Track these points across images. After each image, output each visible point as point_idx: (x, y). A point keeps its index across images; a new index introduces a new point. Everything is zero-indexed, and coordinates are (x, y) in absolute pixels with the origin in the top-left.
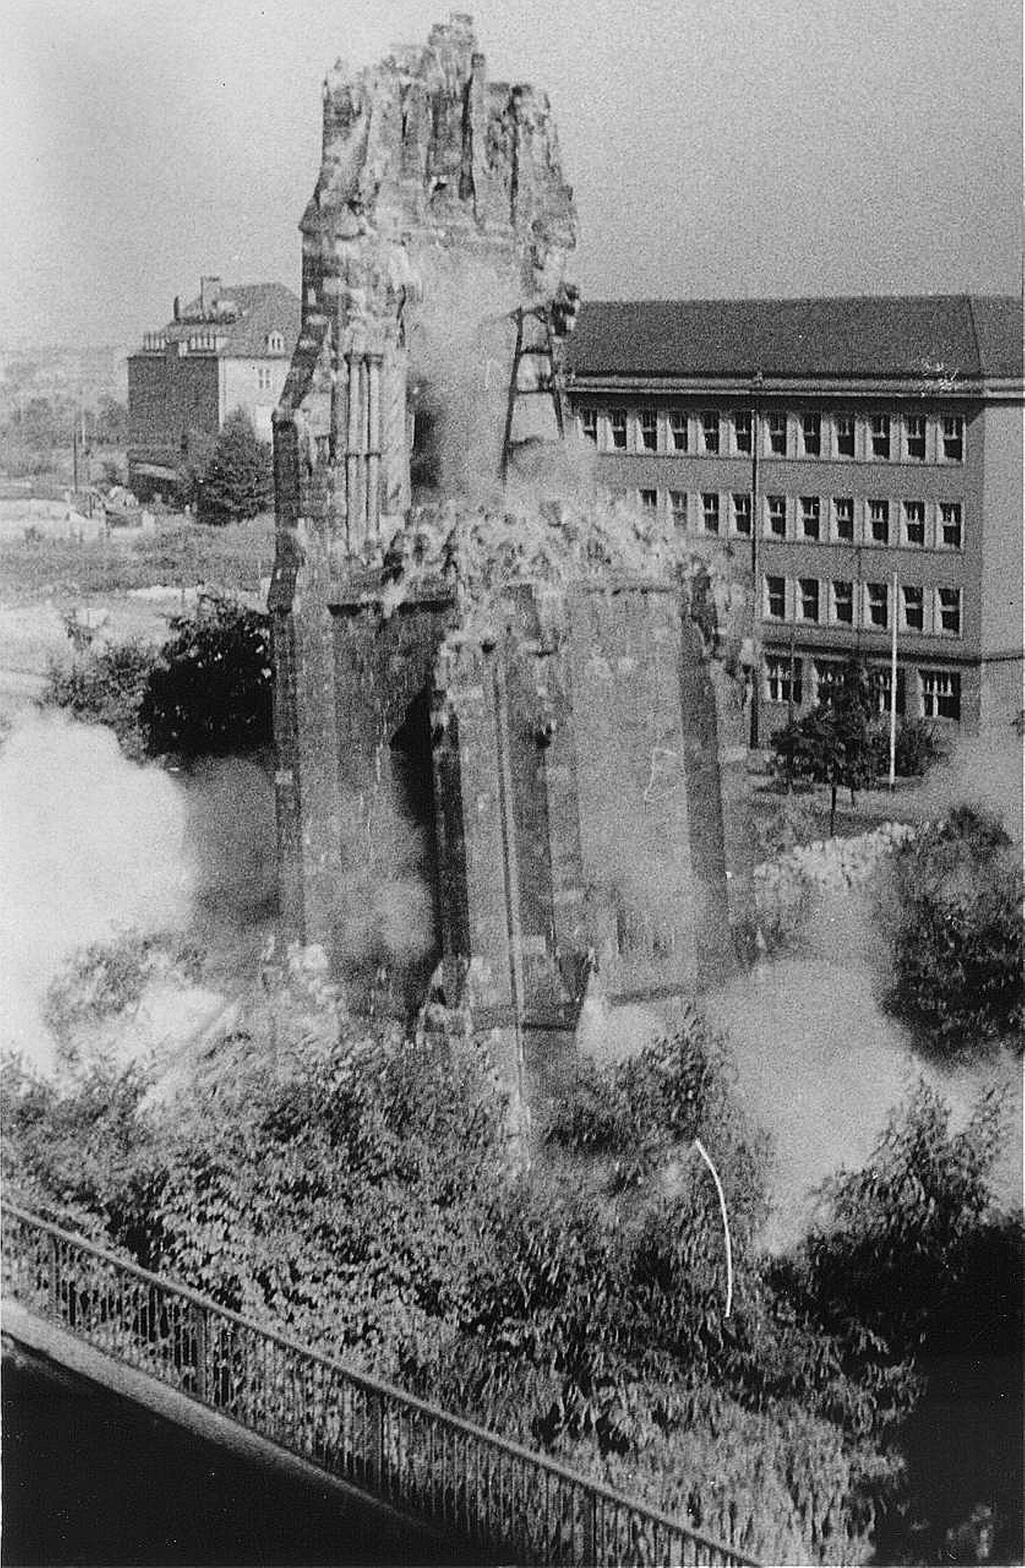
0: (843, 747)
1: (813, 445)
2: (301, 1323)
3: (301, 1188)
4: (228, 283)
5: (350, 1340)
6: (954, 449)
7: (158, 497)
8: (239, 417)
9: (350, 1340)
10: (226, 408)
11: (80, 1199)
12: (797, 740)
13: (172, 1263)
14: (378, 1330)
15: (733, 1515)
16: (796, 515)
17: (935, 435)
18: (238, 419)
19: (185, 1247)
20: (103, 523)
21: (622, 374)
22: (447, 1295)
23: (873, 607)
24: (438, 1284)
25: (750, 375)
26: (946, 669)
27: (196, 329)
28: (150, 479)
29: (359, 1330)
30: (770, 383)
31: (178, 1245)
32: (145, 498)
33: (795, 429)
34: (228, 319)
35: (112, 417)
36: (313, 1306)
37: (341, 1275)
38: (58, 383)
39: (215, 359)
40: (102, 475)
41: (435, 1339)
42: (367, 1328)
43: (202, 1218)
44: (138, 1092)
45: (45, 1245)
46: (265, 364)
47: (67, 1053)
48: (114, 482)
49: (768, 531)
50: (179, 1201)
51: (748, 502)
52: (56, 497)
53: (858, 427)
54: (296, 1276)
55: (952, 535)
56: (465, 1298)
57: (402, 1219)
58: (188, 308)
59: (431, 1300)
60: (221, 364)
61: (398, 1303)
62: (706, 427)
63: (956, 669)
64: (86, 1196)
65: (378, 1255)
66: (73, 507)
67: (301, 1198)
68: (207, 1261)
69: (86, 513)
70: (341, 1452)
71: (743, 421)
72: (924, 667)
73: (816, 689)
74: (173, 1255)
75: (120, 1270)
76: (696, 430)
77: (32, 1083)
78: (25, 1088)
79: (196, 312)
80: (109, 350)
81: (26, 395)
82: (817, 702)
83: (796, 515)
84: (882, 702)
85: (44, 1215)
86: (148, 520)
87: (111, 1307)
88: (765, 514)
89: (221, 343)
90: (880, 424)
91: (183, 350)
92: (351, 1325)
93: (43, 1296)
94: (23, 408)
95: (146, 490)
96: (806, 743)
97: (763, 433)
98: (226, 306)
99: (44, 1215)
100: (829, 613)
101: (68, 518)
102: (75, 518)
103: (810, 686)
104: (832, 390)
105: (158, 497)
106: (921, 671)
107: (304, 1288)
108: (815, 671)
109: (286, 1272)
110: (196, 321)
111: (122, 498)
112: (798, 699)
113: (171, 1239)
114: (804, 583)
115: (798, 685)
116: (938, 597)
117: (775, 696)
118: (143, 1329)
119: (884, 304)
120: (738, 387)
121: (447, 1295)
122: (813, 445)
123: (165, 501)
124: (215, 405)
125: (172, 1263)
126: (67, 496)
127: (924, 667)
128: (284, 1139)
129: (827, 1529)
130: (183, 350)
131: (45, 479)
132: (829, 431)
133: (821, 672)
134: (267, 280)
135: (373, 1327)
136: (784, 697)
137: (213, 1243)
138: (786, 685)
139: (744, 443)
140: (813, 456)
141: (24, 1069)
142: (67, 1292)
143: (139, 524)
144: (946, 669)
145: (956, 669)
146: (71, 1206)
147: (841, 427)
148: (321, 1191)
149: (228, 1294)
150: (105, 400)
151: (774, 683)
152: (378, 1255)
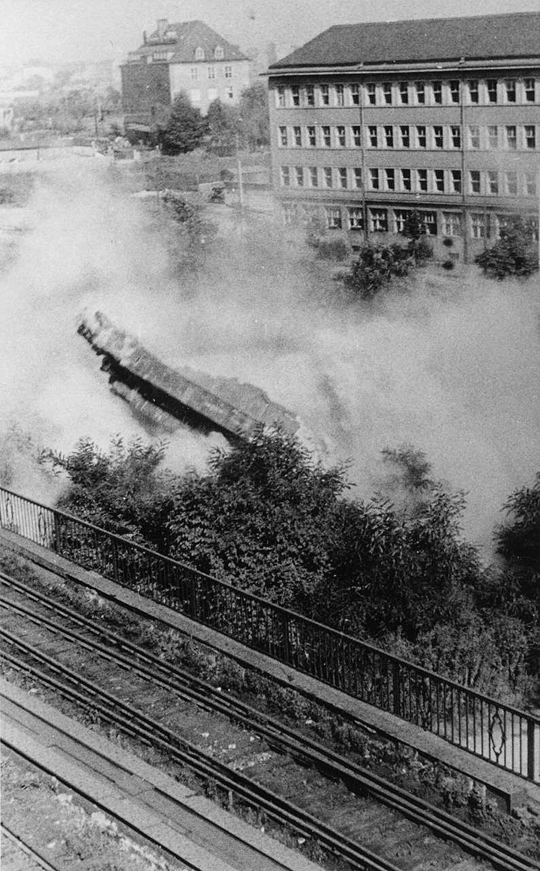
0: (514, 262)
1: (493, 97)
2: (242, 577)
3: (240, 508)
4: (171, 22)
5: (269, 584)
6: (531, 96)
7: (141, 141)
8: (181, 96)
9: (269, 584)
10: (174, 91)
11: (126, 518)
12: (488, 259)
13: (176, 548)
14: (283, 579)
15: (471, 669)
16: (431, 136)
17: (521, 89)
18: (182, 97)
19: (181, 541)
20: (113, 157)
21: (389, 63)
22: (318, 560)
23: (473, 183)
24: (313, 555)
25: (458, 59)
26: (429, 209)
27: (157, 48)
28: (137, 132)
29: (273, 580)
30: (469, 63)
31: (178, 539)
32: (134, 142)
33: (483, 89)
34: (173, 42)
35: (114, 97)
36: (249, 568)
37: (262, 552)
38: (84, 82)
39: (167, 65)
40: (112, 131)
41: (312, 582)
42: (277, 578)
43: (191, 526)
44: (155, 462)
45: (109, 542)
46: (194, 66)
47: (117, 443)
48: (118, 134)
49: (369, 144)
50: (179, 518)
51: (459, 130)
52: (87, 144)
53: (518, 85)
54: (240, 553)
55: (531, 142)
56: (327, 562)
57: (292, 523)
58: (152, 36)
59: (310, 563)
60: (171, 67)
61: (292, 566)
62: (453, 89)
63: (434, 210)
64: (129, 515)
65: (281, 542)
66: (96, 149)
67: (240, 514)
68: (193, 548)
69: (104, 152)
70: (267, 643)
71: (454, 86)
72: (396, 208)
73: (498, 231)
74: (176, 544)
75: (148, 554)
76: (380, 92)
77: (99, 458)
78: (95, 461)
79: (156, 39)
80: (109, 62)
81: (67, 89)
82: (499, 238)
83: (431, 136)
84: (534, 236)
85: (108, 527)
86: (137, 155)
87: (145, 572)
88: (367, 134)
89: (169, 56)
90: (371, 87)
91: (150, 60)
92: (269, 577)
93: (110, 567)
94: (66, 97)
95: (136, 138)
96: (494, 261)
97: (465, 90)
98: (172, 35)
99: (108, 527)
100: (400, 186)
101: (94, 155)
102: (98, 155)
103: (495, 228)
104: (477, 67)
105: (141, 141)
106: (395, 210)
107: (245, 559)
108: (497, 221)
109: (235, 551)
110: (157, 44)
111: (122, 143)
112: (488, 236)
113: (175, 536)
114: (297, 168)
115: (489, 228)
116: (451, 175)
117: (476, 235)
118: (163, 583)
119: (529, 16)
120: (452, 66)
121: (318, 560)
122: (493, 97)
123: (145, 144)
124: (168, 91)
125: (176, 548)
126: (93, 143)
127: (396, 208)
128: (230, 484)
129: (517, 672)
130: (150, 60)
131: (79, 135)
132: (502, 89)
133: (501, 221)
134: (194, 19)
135: (280, 578)
136: (482, 236)
137: (193, 537)
138: (482, 228)
139: (456, 97)
140: (493, 103)
141: (95, 451)
142: (121, 564)
143: (132, 157)
144: (429, 209)
145: (434, 210)
146: (122, 521)
147: (509, 86)
148: (250, 509)
149: (204, 563)
150: (110, 88)
151: (475, 227)
152: (281, 542)
